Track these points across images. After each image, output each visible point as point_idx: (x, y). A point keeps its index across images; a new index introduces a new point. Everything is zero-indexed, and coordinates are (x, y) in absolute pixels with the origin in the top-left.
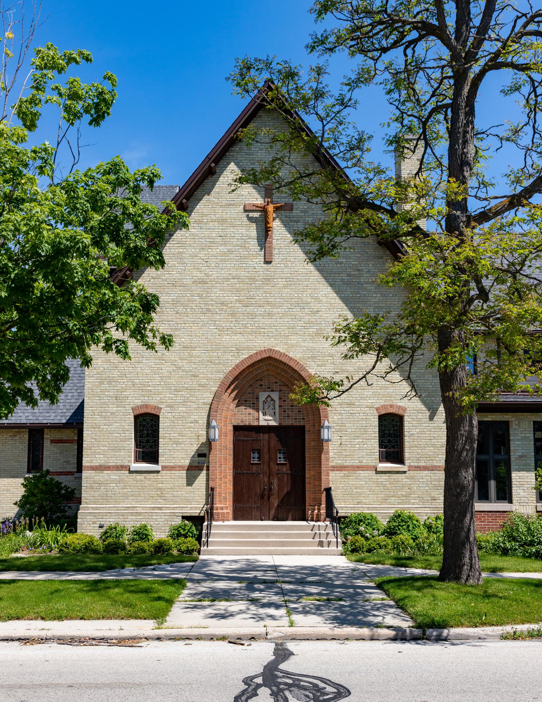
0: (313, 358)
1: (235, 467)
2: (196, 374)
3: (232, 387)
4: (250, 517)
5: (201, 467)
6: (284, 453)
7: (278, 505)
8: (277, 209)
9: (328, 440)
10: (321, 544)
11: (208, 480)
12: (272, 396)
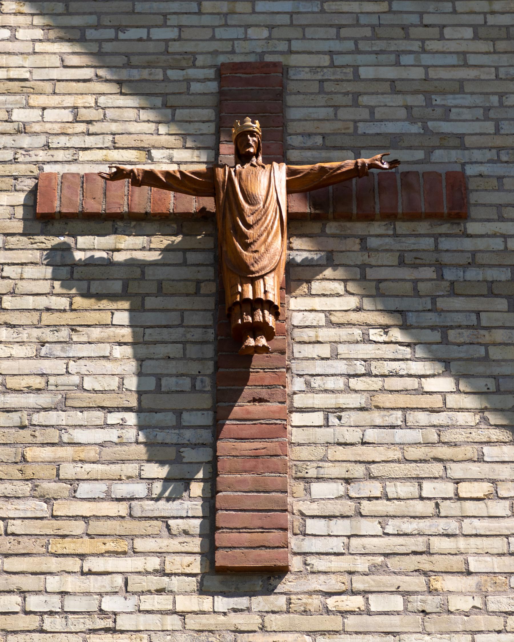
8: (326, 204)
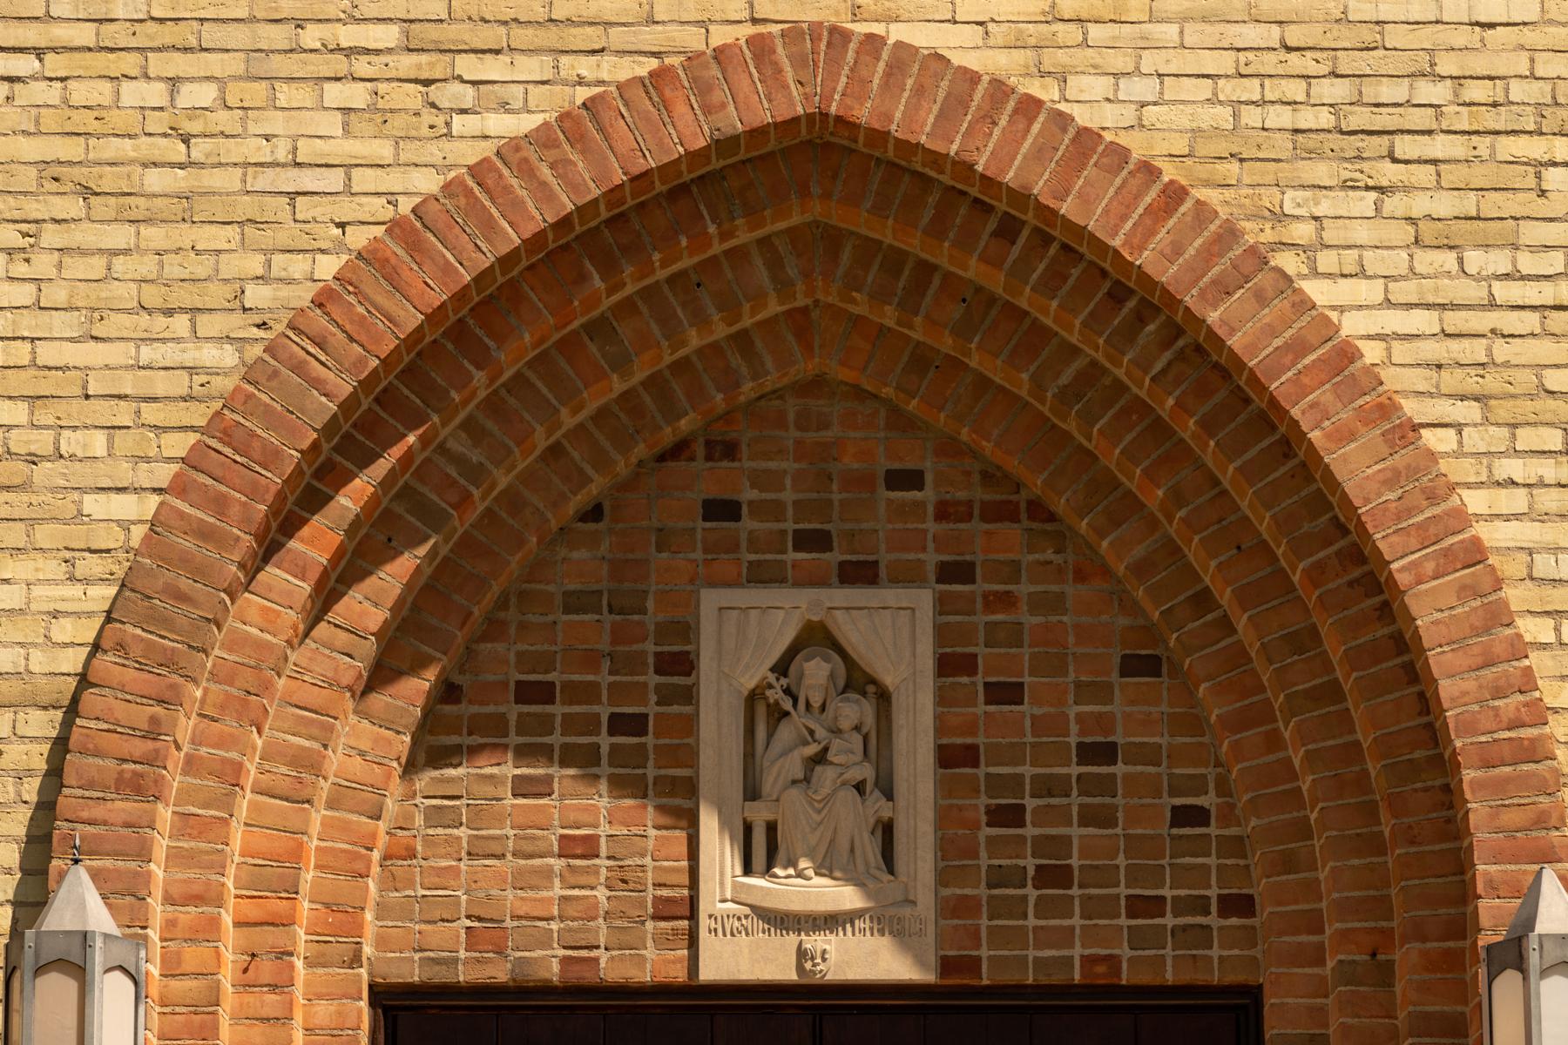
0: (1363, 142)
12: (853, 632)
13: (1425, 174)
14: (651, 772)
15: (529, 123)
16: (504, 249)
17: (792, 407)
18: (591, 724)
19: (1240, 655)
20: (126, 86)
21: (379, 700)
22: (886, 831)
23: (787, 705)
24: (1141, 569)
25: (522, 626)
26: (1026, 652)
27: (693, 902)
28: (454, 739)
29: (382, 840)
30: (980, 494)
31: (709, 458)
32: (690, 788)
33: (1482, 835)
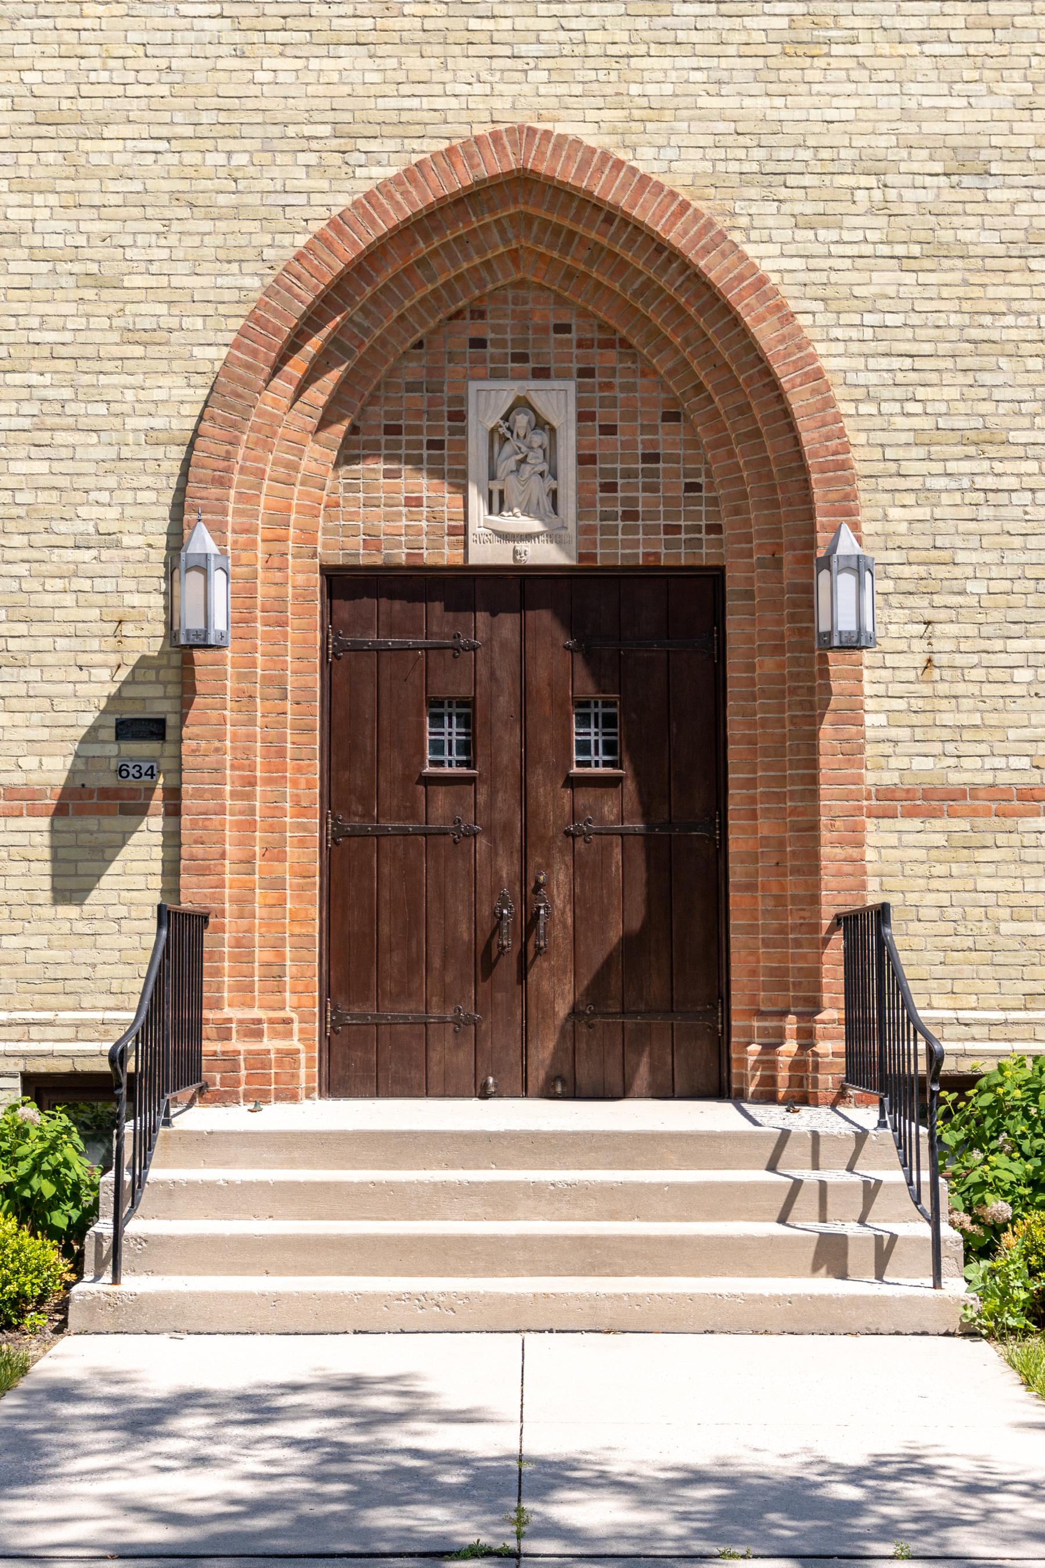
0: (773, 177)
1: (335, 795)
2: (108, 270)
3: (312, 347)
4: (416, 1076)
5: (134, 793)
6: (609, 721)
7: (575, 1012)
9: (855, 643)
10: (831, 1255)
11: (172, 870)
12: (539, 401)
13: (800, 194)
14: (446, 467)
15: (391, 172)
16: (380, 234)
17: (510, 294)
18: (418, 445)
19: (716, 413)
20: (208, 155)
21: (323, 435)
22: (554, 493)
23: (509, 435)
24: (671, 373)
25: (387, 399)
26: (618, 410)
27: (466, 527)
28: (357, 452)
29: (325, 498)
30: (597, 335)
31: (472, 318)
32: (464, 474)
33: (819, 504)
